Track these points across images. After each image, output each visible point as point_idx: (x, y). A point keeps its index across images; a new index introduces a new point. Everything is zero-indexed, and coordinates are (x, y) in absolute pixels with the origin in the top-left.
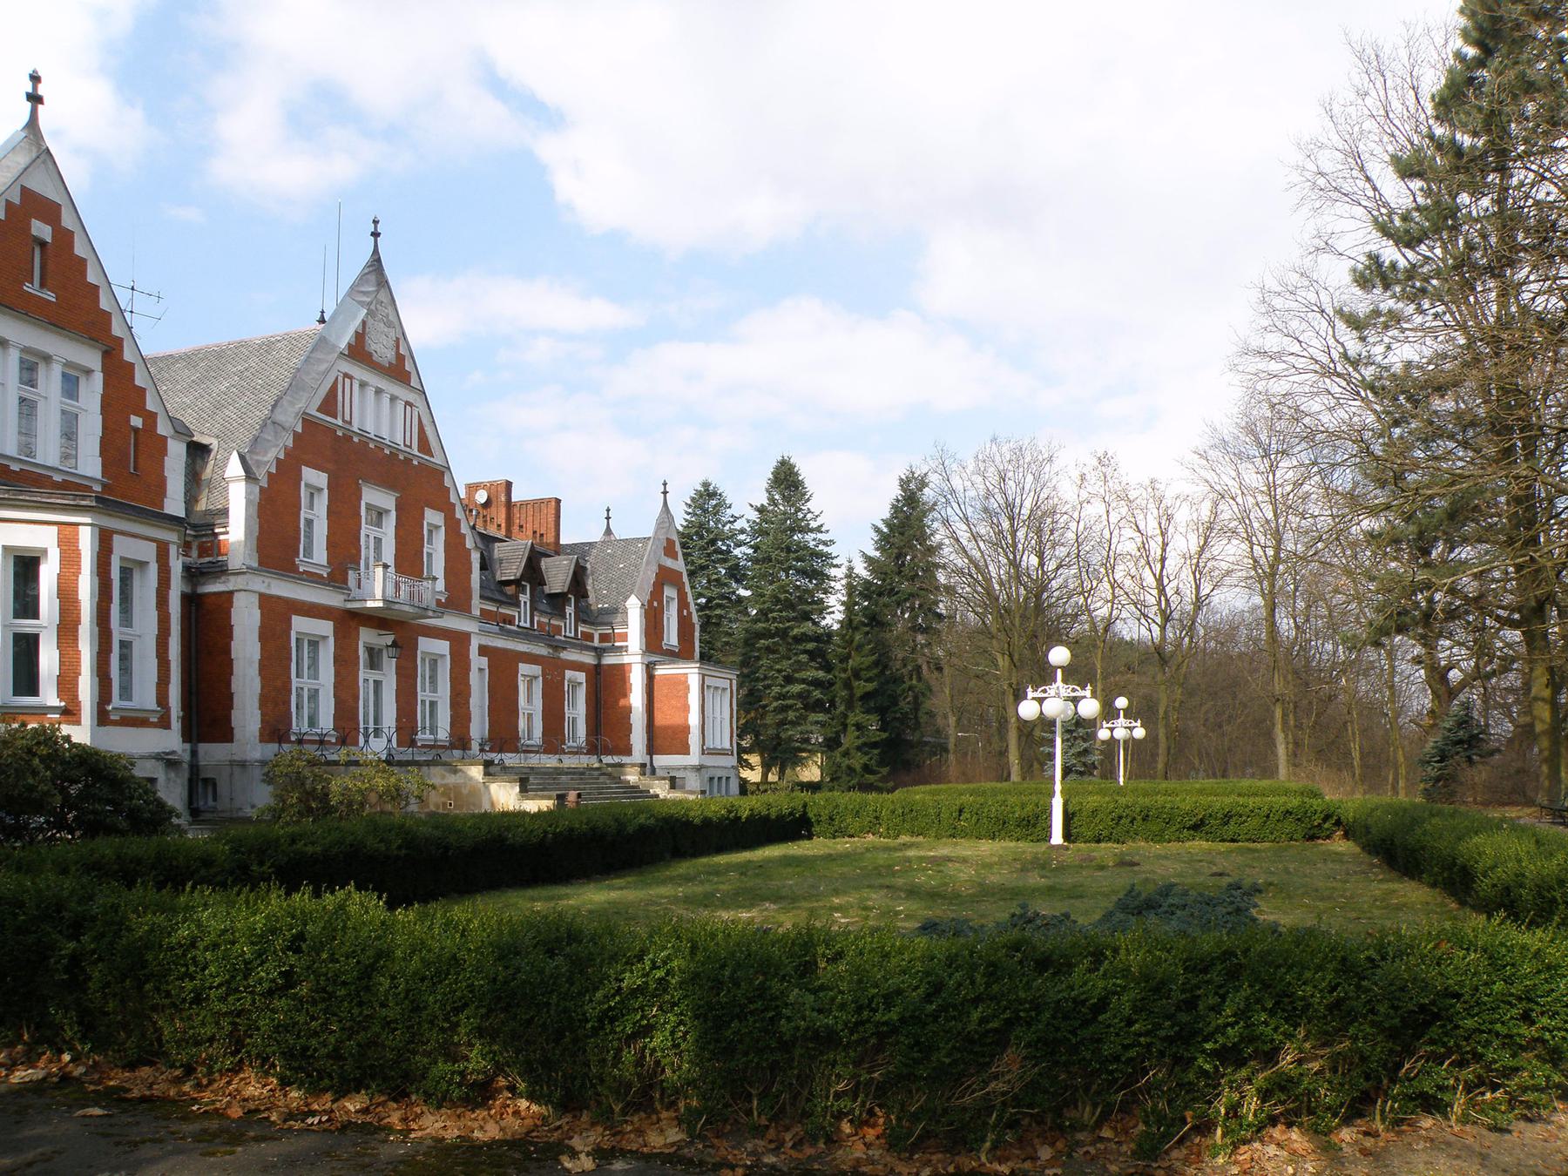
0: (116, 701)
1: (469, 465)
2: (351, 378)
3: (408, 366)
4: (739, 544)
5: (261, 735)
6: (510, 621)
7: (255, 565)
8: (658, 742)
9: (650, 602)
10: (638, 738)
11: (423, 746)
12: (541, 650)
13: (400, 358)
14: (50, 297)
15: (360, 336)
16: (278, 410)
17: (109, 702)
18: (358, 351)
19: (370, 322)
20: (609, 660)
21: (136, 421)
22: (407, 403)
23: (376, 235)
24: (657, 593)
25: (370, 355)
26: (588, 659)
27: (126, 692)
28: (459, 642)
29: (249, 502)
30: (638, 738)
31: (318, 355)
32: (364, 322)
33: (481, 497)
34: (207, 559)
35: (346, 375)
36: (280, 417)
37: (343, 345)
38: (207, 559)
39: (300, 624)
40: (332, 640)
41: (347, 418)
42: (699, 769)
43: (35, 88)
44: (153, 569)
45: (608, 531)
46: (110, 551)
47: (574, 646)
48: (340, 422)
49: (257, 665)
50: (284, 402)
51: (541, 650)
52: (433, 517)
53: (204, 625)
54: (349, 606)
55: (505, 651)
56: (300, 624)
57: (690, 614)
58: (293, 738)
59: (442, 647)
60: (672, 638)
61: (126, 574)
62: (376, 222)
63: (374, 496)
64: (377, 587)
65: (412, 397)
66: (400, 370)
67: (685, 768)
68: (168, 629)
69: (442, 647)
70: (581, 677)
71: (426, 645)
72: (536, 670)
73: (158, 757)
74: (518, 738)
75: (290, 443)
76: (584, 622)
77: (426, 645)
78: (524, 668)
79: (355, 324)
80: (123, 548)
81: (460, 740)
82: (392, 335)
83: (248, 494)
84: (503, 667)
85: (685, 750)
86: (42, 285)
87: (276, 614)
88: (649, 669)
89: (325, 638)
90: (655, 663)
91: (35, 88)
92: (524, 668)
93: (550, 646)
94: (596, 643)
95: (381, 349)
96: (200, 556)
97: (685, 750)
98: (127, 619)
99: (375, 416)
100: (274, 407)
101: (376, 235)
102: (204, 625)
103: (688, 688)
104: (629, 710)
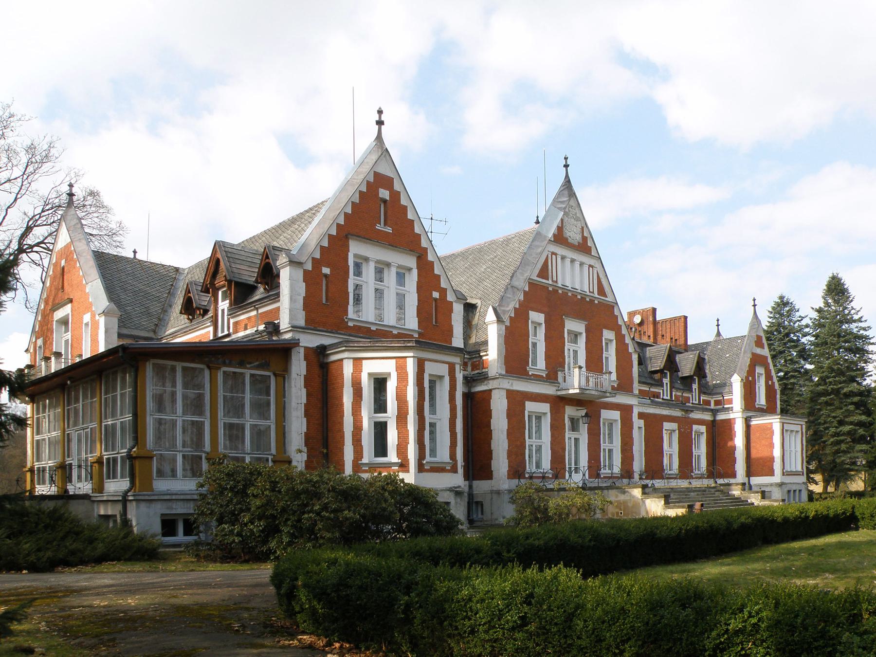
0: (428, 458)
1: (629, 301)
2: (556, 254)
3: (590, 244)
4: (805, 335)
5: (508, 474)
6: (657, 395)
7: (504, 373)
8: (753, 469)
9: (747, 378)
10: (740, 467)
11: (605, 477)
12: (678, 413)
13: (585, 239)
14: (389, 230)
15: (560, 229)
16: (514, 278)
17: (424, 458)
18: (560, 238)
19: (566, 219)
20: (721, 417)
21: (436, 295)
22: (590, 266)
23: (566, 166)
24: (751, 371)
25: (567, 239)
26: (708, 417)
27: (433, 452)
28: (627, 410)
29: (499, 336)
30: (740, 467)
31: (536, 243)
32: (562, 220)
33: (637, 319)
34: (477, 372)
35: (553, 253)
36: (516, 283)
37: (550, 235)
38: (477, 372)
39: (531, 406)
40: (549, 415)
41: (555, 279)
42: (781, 485)
43: (380, 117)
44: (447, 379)
45: (719, 334)
46: (424, 371)
47: (698, 409)
48: (550, 282)
49: (505, 433)
50: (518, 273)
51: (678, 413)
52: (608, 334)
53: (476, 410)
54: (559, 393)
55: (655, 415)
56: (531, 406)
57: (773, 383)
58: (527, 476)
59: (616, 415)
60: (761, 400)
61: (432, 383)
62: (566, 158)
63: (573, 325)
64: (575, 381)
65: (592, 262)
66: (585, 247)
67: (771, 485)
68: (456, 414)
69: (616, 415)
70: (703, 429)
71: (606, 414)
72: (674, 426)
73: (451, 490)
74: (663, 470)
75: (522, 298)
76: (705, 393)
77: (606, 414)
78: (667, 426)
79: (557, 222)
80: (431, 369)
81: (627, 473)
82: (579, 225)
83: (499, 330)
84: (653, 425)
85: (771, 473)
86: (385, 224)
87: (517, 401)
88: (747, 421)
89: (545, 414)
90: (751, 417)
91: (380, 117)
92: (667, 426)
93: (683, 410)
94: (712, 406)
95: (573, 234)
96: (473, 370)
97: (771, 473)
98: (433, 410)
99: (571, 277)
100: (512, 277)
101: (566, 166)
102: (476, 410)
103: (772, 432)
104: (734, 448)
